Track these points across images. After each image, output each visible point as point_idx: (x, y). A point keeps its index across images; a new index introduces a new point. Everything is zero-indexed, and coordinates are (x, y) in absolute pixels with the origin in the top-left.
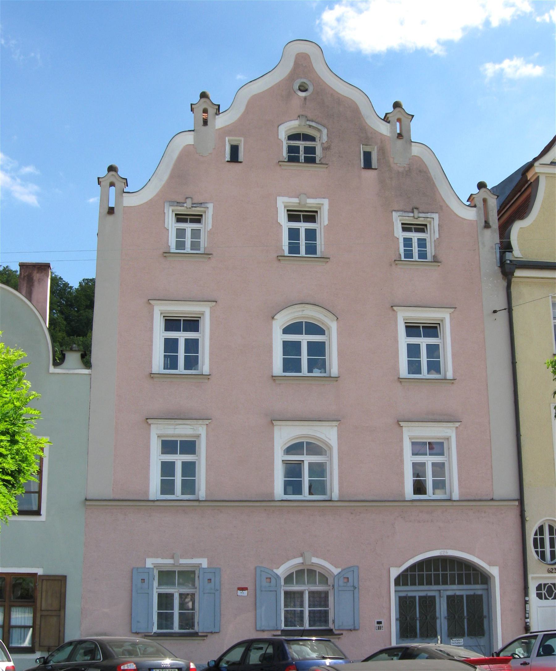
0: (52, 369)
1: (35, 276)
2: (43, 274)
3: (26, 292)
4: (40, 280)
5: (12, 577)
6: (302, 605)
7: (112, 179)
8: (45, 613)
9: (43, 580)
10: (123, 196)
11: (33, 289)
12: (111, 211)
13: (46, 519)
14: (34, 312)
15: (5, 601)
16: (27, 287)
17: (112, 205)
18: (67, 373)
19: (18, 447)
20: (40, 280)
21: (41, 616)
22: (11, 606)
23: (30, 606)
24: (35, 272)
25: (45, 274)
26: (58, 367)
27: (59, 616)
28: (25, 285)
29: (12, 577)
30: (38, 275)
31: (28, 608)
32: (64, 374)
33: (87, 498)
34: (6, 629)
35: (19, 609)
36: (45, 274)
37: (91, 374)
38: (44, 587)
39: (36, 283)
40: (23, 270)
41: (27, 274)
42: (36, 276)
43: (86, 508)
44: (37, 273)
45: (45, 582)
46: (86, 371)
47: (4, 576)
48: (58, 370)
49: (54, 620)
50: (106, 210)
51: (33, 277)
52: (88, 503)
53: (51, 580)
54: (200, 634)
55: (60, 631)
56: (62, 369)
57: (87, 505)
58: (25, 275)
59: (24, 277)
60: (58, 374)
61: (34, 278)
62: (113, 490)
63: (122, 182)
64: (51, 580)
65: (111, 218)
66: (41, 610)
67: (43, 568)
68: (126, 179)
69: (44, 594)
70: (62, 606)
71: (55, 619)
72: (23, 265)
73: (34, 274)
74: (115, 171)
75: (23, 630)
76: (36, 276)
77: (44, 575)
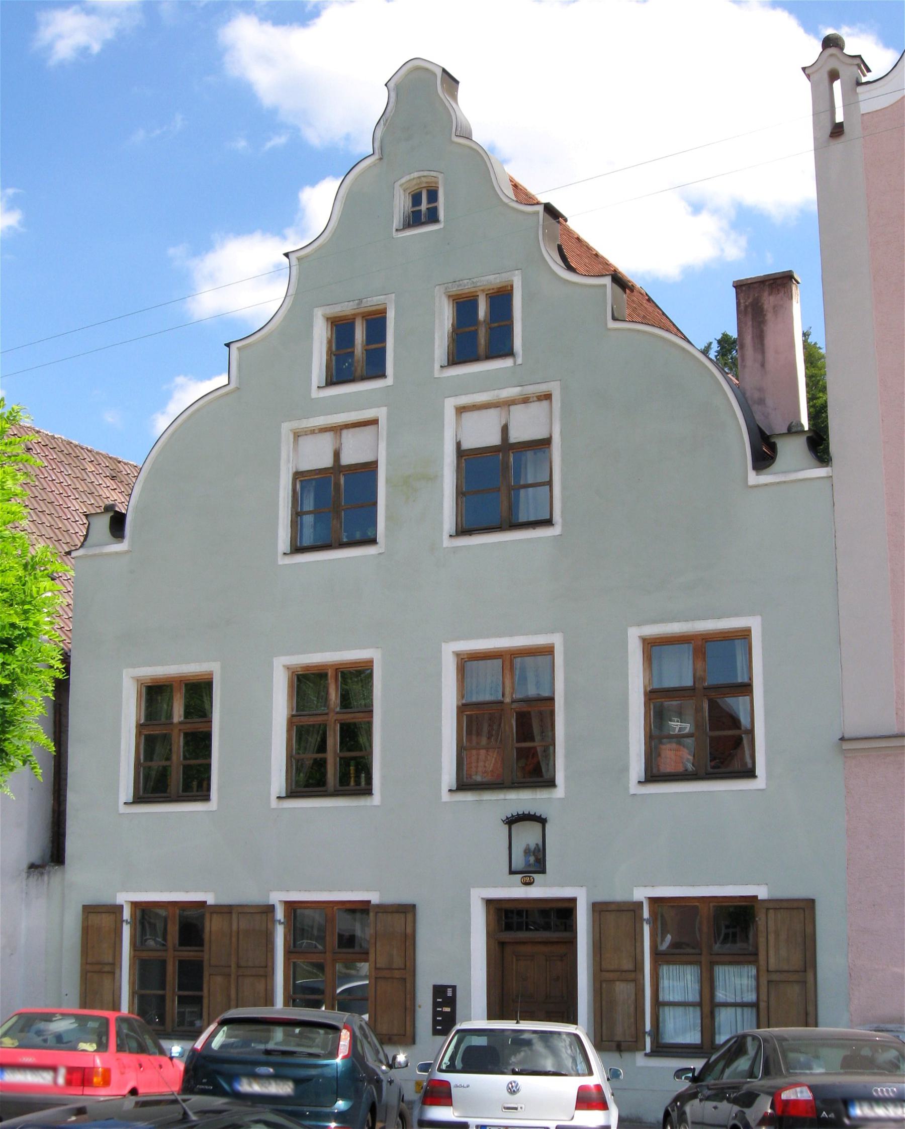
0: (753, 478)
1: (766, 303)
2: (782, 294)
3: (753, 338)
4: (776, 309)
5: (711, 905)
6: (163, 986)
7: (833, 64)
8: (775, 977)
9: (768, 909)
10: (857, 94)
11: (765, 328)
12: (837, 130)
13: (766, 784)
14: (706, 367)
15: (700, 954)
16: (753, 327)
17: (839, 118)
18: (785, 482)
19: (18, 622)
20: (776, 308)
21: (769, 982)
22: (712, 964)
23: (749, 963)
24: (766, 294)
25: (785, 293)
26: (764, 471)
27: (805, 982)
28: (750, 323)
29: (711, 905)
30: (772, 298)
31: (746, 966)
32: (778, 483)
33: (847, 736)
34: (707, 1009)
35: (750, 969)
36: (785, 293)
37: (832, 477)
38: (771, 924)
39: (769, 316)
40: (742, 295)
41: (750, 300)
42: (769, 301)
43: (845, 757)
44: (770, 294)
45: (771, 912)
46: (822, 472)
47: (697, 904)
48: (765, 478)
49: (794, 992)
50: (828, 129)
51: (763, 304)
52: (846, 746)
53: (784, 909)
54: (280, 1053)
55: (807, 1014)
56: (771, 474)
57: (845, 750)
58: (747, 303)
59: (746, 307)
60: (766, 485)
61: (765, 307)
62: (897, 714)
63: (853, 65)
64: (784, 909)
65: (838, 145)
66: (768, 971)
67: (767, 884)
68: (859, 57)
69: (772, 938)
70: (809, 963)
71: (797, 988)
72: (741, 286)
73: (764, 298)
74: (836, 47)
75: (739, 1010)
76: (769, 301)
77: (216, 904)
